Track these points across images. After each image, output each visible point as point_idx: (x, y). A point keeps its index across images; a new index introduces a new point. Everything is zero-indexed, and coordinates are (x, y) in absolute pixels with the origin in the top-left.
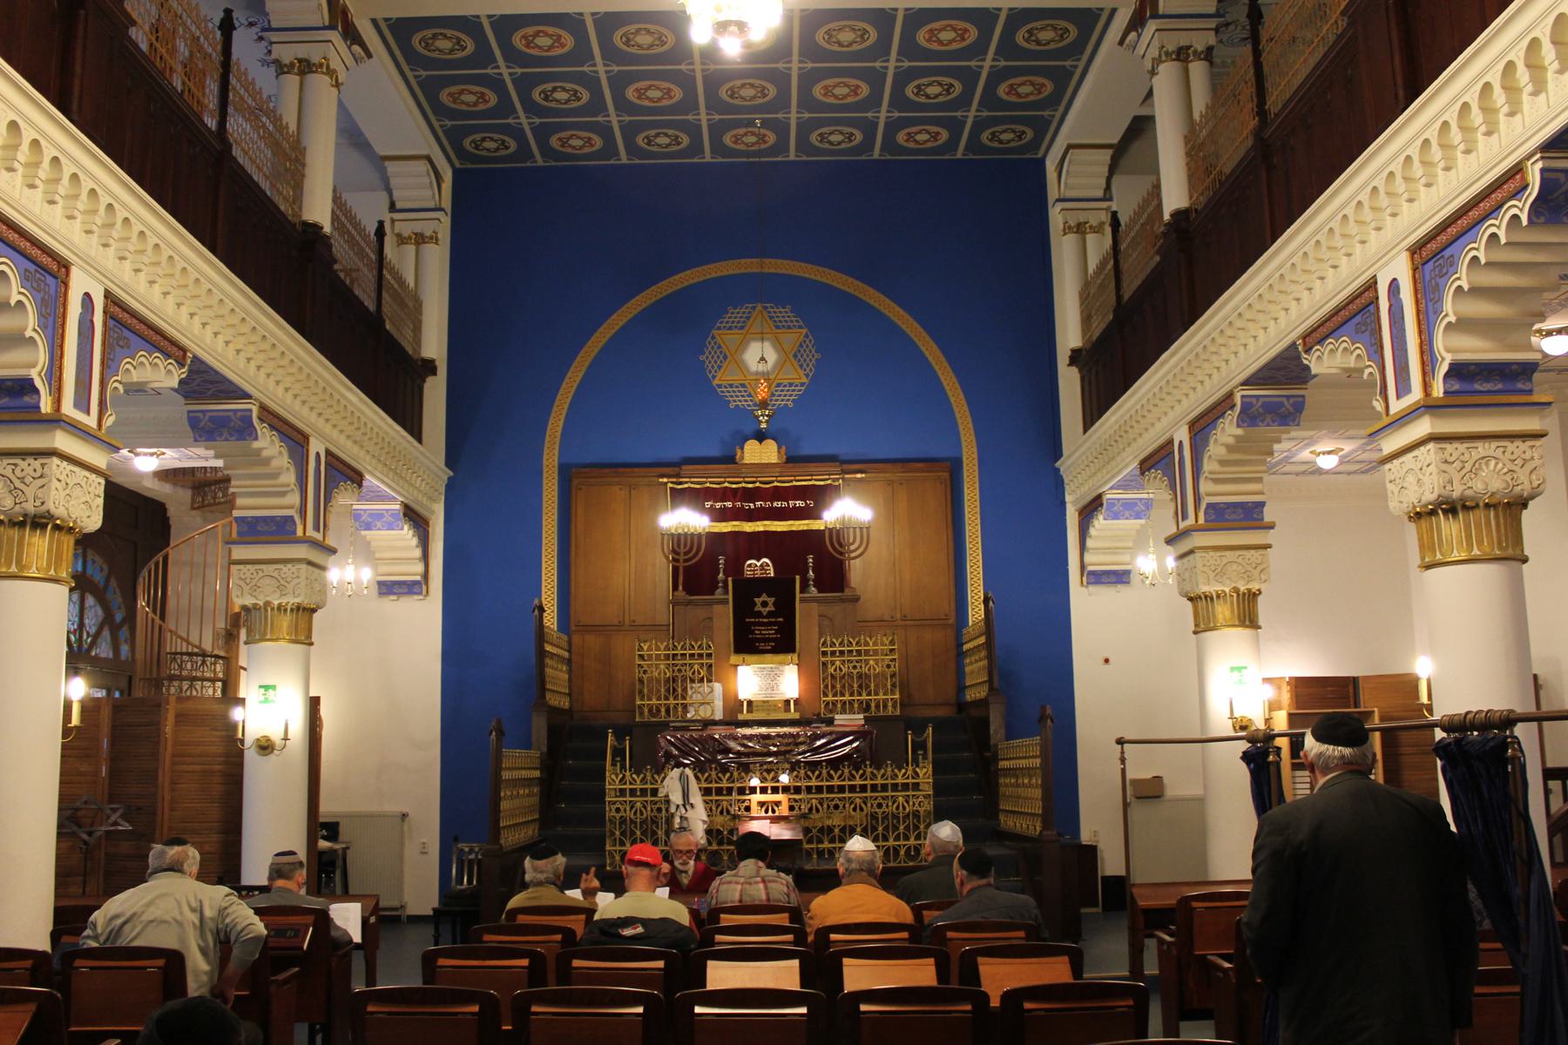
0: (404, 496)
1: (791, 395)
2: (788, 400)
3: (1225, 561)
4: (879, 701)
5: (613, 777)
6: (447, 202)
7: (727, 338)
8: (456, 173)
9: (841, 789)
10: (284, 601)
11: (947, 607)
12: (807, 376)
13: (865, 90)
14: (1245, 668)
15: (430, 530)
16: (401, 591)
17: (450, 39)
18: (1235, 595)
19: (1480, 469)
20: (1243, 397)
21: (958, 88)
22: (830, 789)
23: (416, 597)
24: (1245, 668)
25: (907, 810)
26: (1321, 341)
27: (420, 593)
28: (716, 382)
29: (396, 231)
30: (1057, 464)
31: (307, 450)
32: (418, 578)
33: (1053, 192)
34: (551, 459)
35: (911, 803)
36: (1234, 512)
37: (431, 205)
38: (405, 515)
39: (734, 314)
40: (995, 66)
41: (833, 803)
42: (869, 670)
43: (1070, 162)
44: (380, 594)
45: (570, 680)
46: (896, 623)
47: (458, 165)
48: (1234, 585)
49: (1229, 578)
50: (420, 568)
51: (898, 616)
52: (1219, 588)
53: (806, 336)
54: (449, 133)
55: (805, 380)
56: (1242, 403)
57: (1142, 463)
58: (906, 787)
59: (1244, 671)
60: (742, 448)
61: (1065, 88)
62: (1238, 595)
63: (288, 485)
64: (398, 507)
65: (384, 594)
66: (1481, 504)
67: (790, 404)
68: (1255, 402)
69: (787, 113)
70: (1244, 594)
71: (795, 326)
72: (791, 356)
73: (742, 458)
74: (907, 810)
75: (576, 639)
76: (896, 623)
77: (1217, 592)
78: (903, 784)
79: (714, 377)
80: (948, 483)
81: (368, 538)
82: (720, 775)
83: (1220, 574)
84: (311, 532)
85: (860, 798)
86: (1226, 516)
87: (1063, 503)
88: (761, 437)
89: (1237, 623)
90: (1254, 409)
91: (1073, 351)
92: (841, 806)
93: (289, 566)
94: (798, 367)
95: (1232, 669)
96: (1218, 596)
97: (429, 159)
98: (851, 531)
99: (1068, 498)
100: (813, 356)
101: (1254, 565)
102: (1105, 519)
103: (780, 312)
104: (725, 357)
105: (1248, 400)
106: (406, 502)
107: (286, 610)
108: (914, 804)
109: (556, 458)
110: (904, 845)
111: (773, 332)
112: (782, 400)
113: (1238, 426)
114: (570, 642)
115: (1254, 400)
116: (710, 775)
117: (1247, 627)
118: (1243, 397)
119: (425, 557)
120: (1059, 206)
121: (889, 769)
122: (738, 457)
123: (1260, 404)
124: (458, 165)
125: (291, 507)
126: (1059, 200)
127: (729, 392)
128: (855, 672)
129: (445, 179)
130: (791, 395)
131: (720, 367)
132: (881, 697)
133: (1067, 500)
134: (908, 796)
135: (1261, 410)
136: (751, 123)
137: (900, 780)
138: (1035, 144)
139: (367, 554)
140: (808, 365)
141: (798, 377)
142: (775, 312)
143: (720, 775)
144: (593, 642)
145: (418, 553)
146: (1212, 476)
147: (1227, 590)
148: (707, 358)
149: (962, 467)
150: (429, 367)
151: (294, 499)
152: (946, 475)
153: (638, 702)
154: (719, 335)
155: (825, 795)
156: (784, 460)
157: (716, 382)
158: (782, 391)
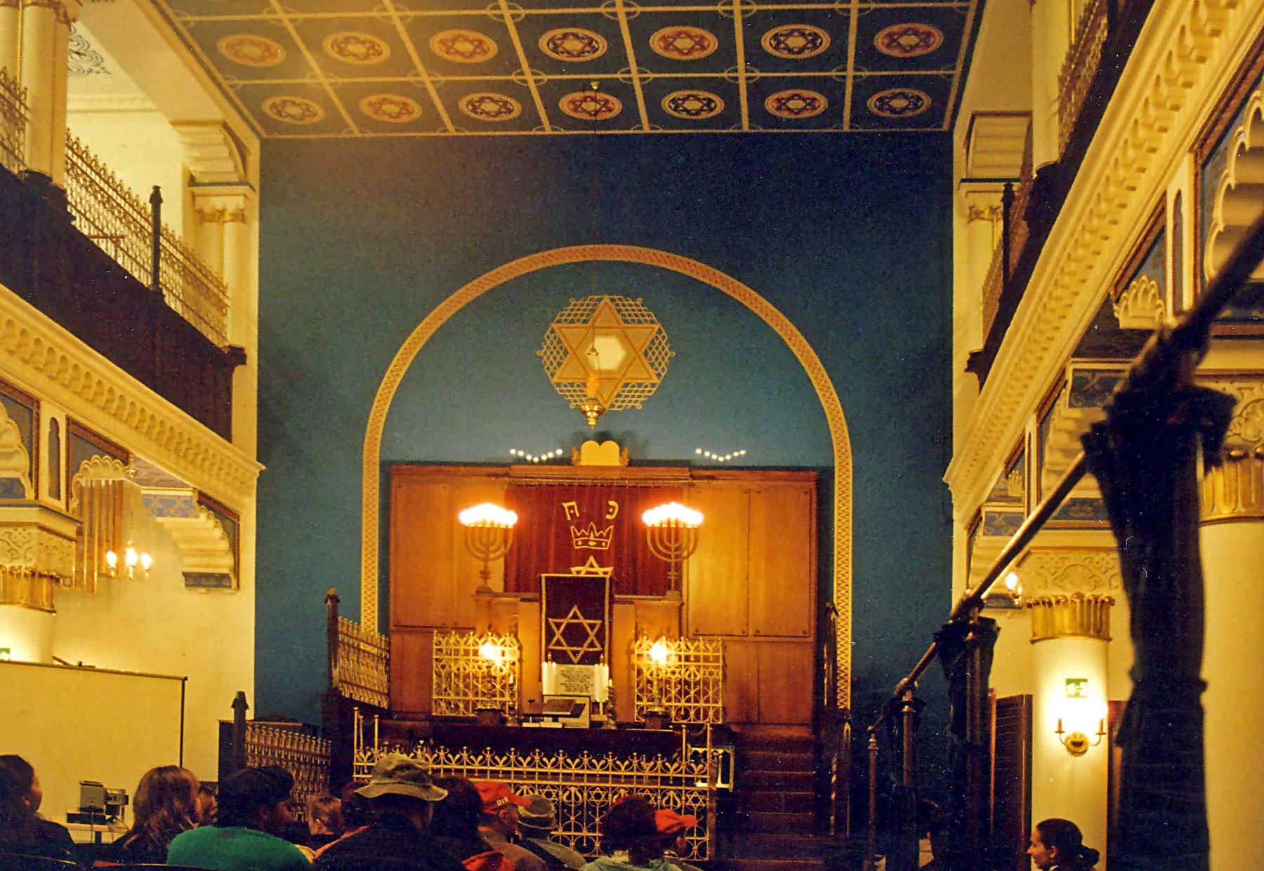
0: (195, 482)
1: (639, 397)
2: (636, 402)
3: (1067, 563)
4: (699, 709)
5: (361, 754)
6: (254, 176)
7: (567, 332)
8: (264, 143)
9: (604, 778)
10: (16, 564)
11: (804, 621)
12: (659, 375)
13: (712, 43)
14: (1085, 681)
15: (241, 523)
16: (207, 583)
17: (363, 42)
18: (1078, 601)
19: (1254, 412)
20: (1075, 370)
21: (826, 40)
22: (592, 777)
23: (227, 591)
24: (1085, 681)
25: (679, 806)
26: (1127, 287)
27: (230, 587)
28: (555, 380)
29: (197, 207)
30: (944, 479)
31: (38, 414)
32: (226, 571)
33: (959, 172)
34: (372, 456)
35: (683, 798)
36: (1081, 511)
37: (235, 178)
38: (200, 503)
39: (576, 306)
40: (866, 10)
41: (595, 792)
42: (689, 676)
43: (976, 138)
44: (187, 585)
45: (389, 681)
46: (749, 639)
47: (264, 135)
48: (1076, 590)
49: (1072, 583)
50: (229, 561)
51: (751, 632)
52: (1059, 593)
53: (660, 332)
54: (242, 94)
55: (655, 380)
56: (1075, 380)
57: (1008, 463)
58: (677, 781)
59: (1082, 684)
60: (579, 450)
61: (960, 33)
62: (1082, 602)
63: (11, 446)
64: (190, 494)
65: (192, 585)
66: (1252, 455)
67: (639, 406)
68: (1090, 378)
69: (644, 79)
70: (1089, 601)
71: (646, 321)
72: (641, 354)
73: (579, 460)
74: (679, 806)
75: (396, 639)
76: (749, 639)
77: (1056, 597)
78: (675, 778)
79: (553, 375)
80: (814, 493)
81: (167, 526)
82: (472, 757)
83: (1060, 578)
84: (45, 498)
85: (626, 789)
86: (1072, 514)
87: (950, 521)
88: (602, 438)
89: (1079, 632)
90: (1089, 386)
91: (973, 355)
92: (603, 796)
93: (20, 529)
94: (649, 367)
95: (1069, 682)
96: (1058, 602)
97: (225, 126)
98: (685, 531)
99: (956, 515)
100: (666, 354)
101: (1103, 570)
102: (984, 534)
103: (630, 305)
104: (566, 353)
105: (1082, 374)
106: (199, 488)
107: (19, 575)
108: (687, 800)
109: (377, 455)
110: (698, 841)
111: (623, 326)
112: (630, 402)
113: (1071, 405)
114: (389, 643)
115: (1089, 375)
116: (461, 757)
117: (1090, 636)
118: (1075, 370)
119: (235, 549)
120: (966, 186)
121: (660, 762)
122: (574, 459)
123: (1095, 380)
124: (264, 135)
125: (17, 470)
126: (963, 181)
127: (569, 391)
128: (674, 677)
129: (252, 150)
130: (639, 397)
131: (559, 364)
132: (702, 704)
133: (954, 518)
134: (681, 791)
135: (1097, 387)
136: (585, 86)
137: (671, 774)
138: (936, 113)
139: (162, 540)
140: (660, 364)
141: (650, 377)
142: (624, 305)
143: (472, 757)
144: (413, 643)
145: (224, 545)
146: (1054, 468)
147: (1068, 595)
148: (545, 353)
149: (833, 478)
150: (238, 355)
151: (22, 461)
152: (812, 485)
153: (435, 697)
154: (560, 329)
155: (585, 784)
156: (626, 463)
157: (555, 380)
158: (630, 391)
